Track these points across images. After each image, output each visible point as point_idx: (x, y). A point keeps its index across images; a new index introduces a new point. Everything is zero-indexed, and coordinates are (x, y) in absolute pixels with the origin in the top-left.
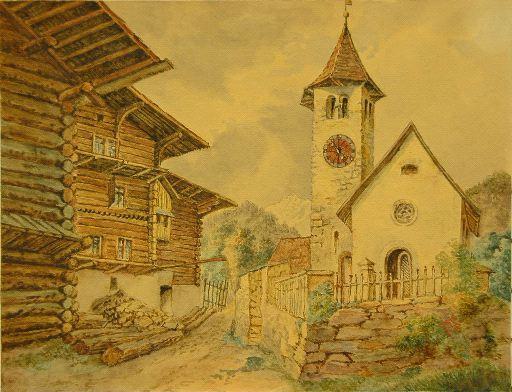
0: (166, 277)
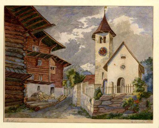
0: (52, 85)
